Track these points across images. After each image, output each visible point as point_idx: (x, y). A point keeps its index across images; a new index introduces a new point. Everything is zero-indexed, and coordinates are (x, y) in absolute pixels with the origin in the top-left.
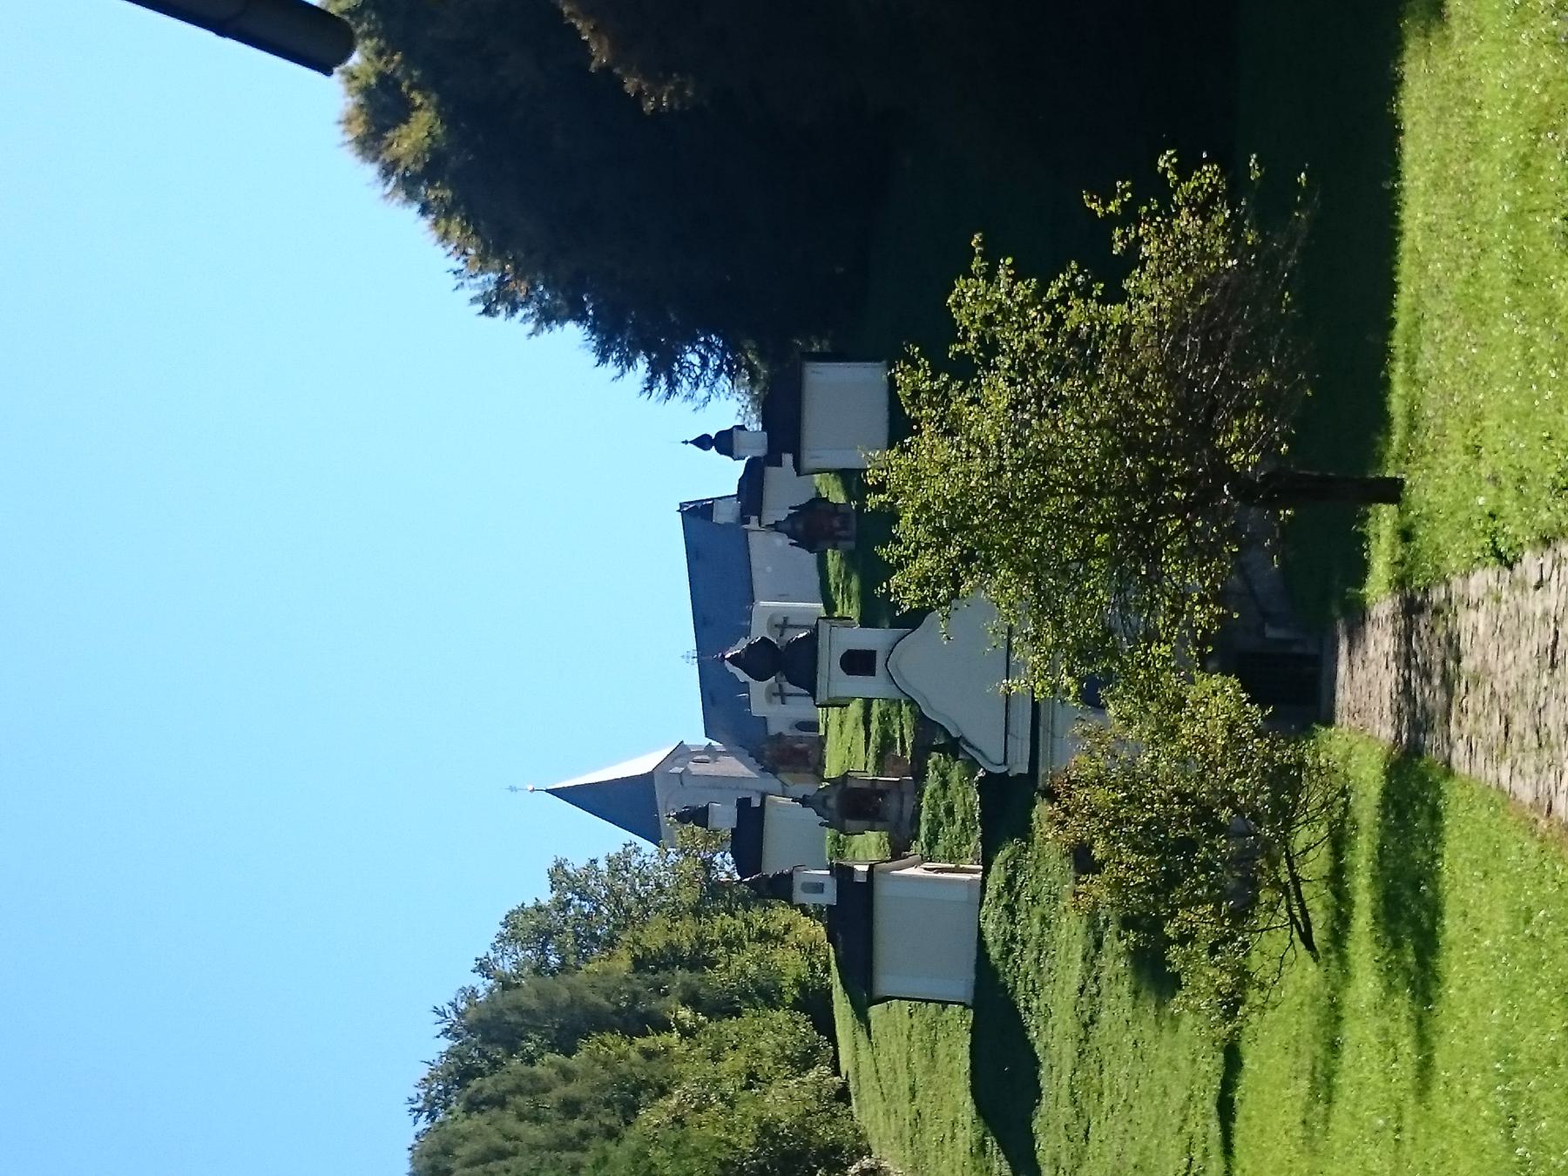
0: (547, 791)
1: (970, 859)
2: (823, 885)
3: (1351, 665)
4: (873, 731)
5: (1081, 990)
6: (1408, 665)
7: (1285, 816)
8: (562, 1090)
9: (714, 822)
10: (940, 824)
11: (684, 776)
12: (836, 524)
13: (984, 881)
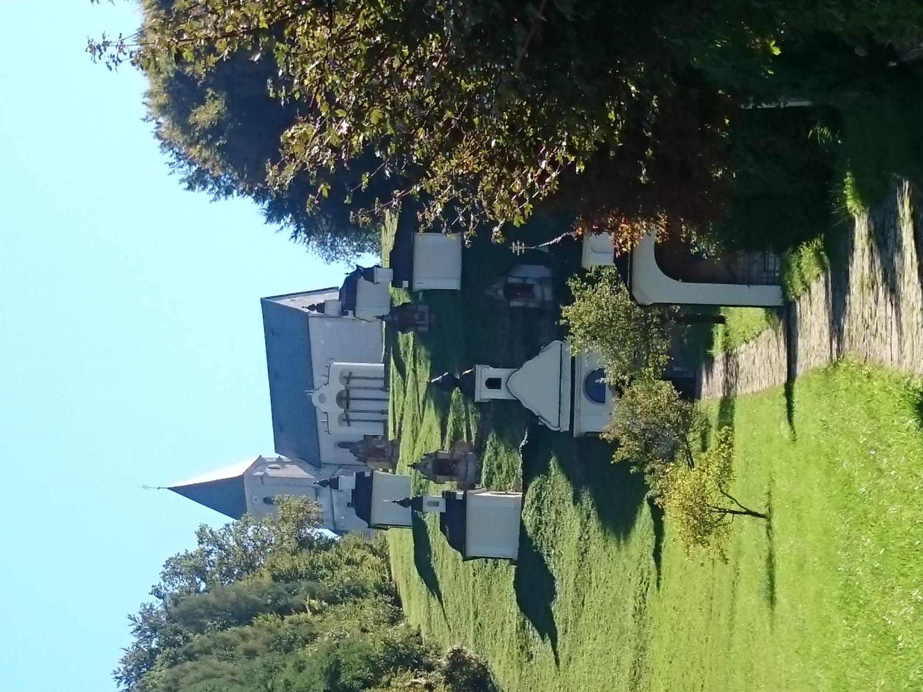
0: (169, 488)
1: (512, 490)
2: (438, 503)
3: (707, 379)
5: (580, 539)
6: (727, 373)
8: (242, 645)
11: (263, 478)
12: (416, 317)
13: (523, 498)
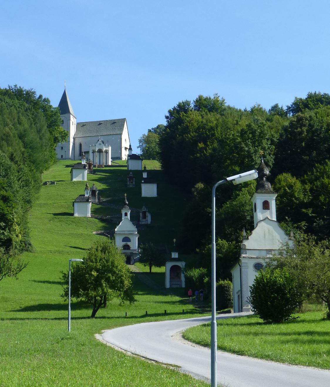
0: (65, 91)
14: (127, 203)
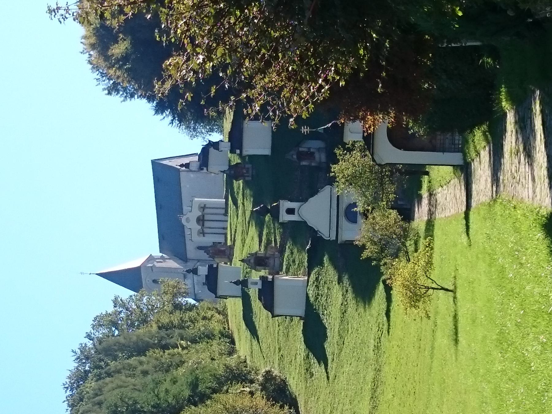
0: (97, 274)
4: (263, 239)
5: (342, 304)
7: (406, 237)
8: (140, 368)
9: (199, 273)
10: (290, 265)
13: (308, 280)
14: (324, 67)
